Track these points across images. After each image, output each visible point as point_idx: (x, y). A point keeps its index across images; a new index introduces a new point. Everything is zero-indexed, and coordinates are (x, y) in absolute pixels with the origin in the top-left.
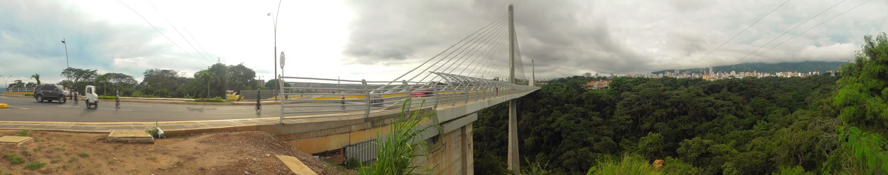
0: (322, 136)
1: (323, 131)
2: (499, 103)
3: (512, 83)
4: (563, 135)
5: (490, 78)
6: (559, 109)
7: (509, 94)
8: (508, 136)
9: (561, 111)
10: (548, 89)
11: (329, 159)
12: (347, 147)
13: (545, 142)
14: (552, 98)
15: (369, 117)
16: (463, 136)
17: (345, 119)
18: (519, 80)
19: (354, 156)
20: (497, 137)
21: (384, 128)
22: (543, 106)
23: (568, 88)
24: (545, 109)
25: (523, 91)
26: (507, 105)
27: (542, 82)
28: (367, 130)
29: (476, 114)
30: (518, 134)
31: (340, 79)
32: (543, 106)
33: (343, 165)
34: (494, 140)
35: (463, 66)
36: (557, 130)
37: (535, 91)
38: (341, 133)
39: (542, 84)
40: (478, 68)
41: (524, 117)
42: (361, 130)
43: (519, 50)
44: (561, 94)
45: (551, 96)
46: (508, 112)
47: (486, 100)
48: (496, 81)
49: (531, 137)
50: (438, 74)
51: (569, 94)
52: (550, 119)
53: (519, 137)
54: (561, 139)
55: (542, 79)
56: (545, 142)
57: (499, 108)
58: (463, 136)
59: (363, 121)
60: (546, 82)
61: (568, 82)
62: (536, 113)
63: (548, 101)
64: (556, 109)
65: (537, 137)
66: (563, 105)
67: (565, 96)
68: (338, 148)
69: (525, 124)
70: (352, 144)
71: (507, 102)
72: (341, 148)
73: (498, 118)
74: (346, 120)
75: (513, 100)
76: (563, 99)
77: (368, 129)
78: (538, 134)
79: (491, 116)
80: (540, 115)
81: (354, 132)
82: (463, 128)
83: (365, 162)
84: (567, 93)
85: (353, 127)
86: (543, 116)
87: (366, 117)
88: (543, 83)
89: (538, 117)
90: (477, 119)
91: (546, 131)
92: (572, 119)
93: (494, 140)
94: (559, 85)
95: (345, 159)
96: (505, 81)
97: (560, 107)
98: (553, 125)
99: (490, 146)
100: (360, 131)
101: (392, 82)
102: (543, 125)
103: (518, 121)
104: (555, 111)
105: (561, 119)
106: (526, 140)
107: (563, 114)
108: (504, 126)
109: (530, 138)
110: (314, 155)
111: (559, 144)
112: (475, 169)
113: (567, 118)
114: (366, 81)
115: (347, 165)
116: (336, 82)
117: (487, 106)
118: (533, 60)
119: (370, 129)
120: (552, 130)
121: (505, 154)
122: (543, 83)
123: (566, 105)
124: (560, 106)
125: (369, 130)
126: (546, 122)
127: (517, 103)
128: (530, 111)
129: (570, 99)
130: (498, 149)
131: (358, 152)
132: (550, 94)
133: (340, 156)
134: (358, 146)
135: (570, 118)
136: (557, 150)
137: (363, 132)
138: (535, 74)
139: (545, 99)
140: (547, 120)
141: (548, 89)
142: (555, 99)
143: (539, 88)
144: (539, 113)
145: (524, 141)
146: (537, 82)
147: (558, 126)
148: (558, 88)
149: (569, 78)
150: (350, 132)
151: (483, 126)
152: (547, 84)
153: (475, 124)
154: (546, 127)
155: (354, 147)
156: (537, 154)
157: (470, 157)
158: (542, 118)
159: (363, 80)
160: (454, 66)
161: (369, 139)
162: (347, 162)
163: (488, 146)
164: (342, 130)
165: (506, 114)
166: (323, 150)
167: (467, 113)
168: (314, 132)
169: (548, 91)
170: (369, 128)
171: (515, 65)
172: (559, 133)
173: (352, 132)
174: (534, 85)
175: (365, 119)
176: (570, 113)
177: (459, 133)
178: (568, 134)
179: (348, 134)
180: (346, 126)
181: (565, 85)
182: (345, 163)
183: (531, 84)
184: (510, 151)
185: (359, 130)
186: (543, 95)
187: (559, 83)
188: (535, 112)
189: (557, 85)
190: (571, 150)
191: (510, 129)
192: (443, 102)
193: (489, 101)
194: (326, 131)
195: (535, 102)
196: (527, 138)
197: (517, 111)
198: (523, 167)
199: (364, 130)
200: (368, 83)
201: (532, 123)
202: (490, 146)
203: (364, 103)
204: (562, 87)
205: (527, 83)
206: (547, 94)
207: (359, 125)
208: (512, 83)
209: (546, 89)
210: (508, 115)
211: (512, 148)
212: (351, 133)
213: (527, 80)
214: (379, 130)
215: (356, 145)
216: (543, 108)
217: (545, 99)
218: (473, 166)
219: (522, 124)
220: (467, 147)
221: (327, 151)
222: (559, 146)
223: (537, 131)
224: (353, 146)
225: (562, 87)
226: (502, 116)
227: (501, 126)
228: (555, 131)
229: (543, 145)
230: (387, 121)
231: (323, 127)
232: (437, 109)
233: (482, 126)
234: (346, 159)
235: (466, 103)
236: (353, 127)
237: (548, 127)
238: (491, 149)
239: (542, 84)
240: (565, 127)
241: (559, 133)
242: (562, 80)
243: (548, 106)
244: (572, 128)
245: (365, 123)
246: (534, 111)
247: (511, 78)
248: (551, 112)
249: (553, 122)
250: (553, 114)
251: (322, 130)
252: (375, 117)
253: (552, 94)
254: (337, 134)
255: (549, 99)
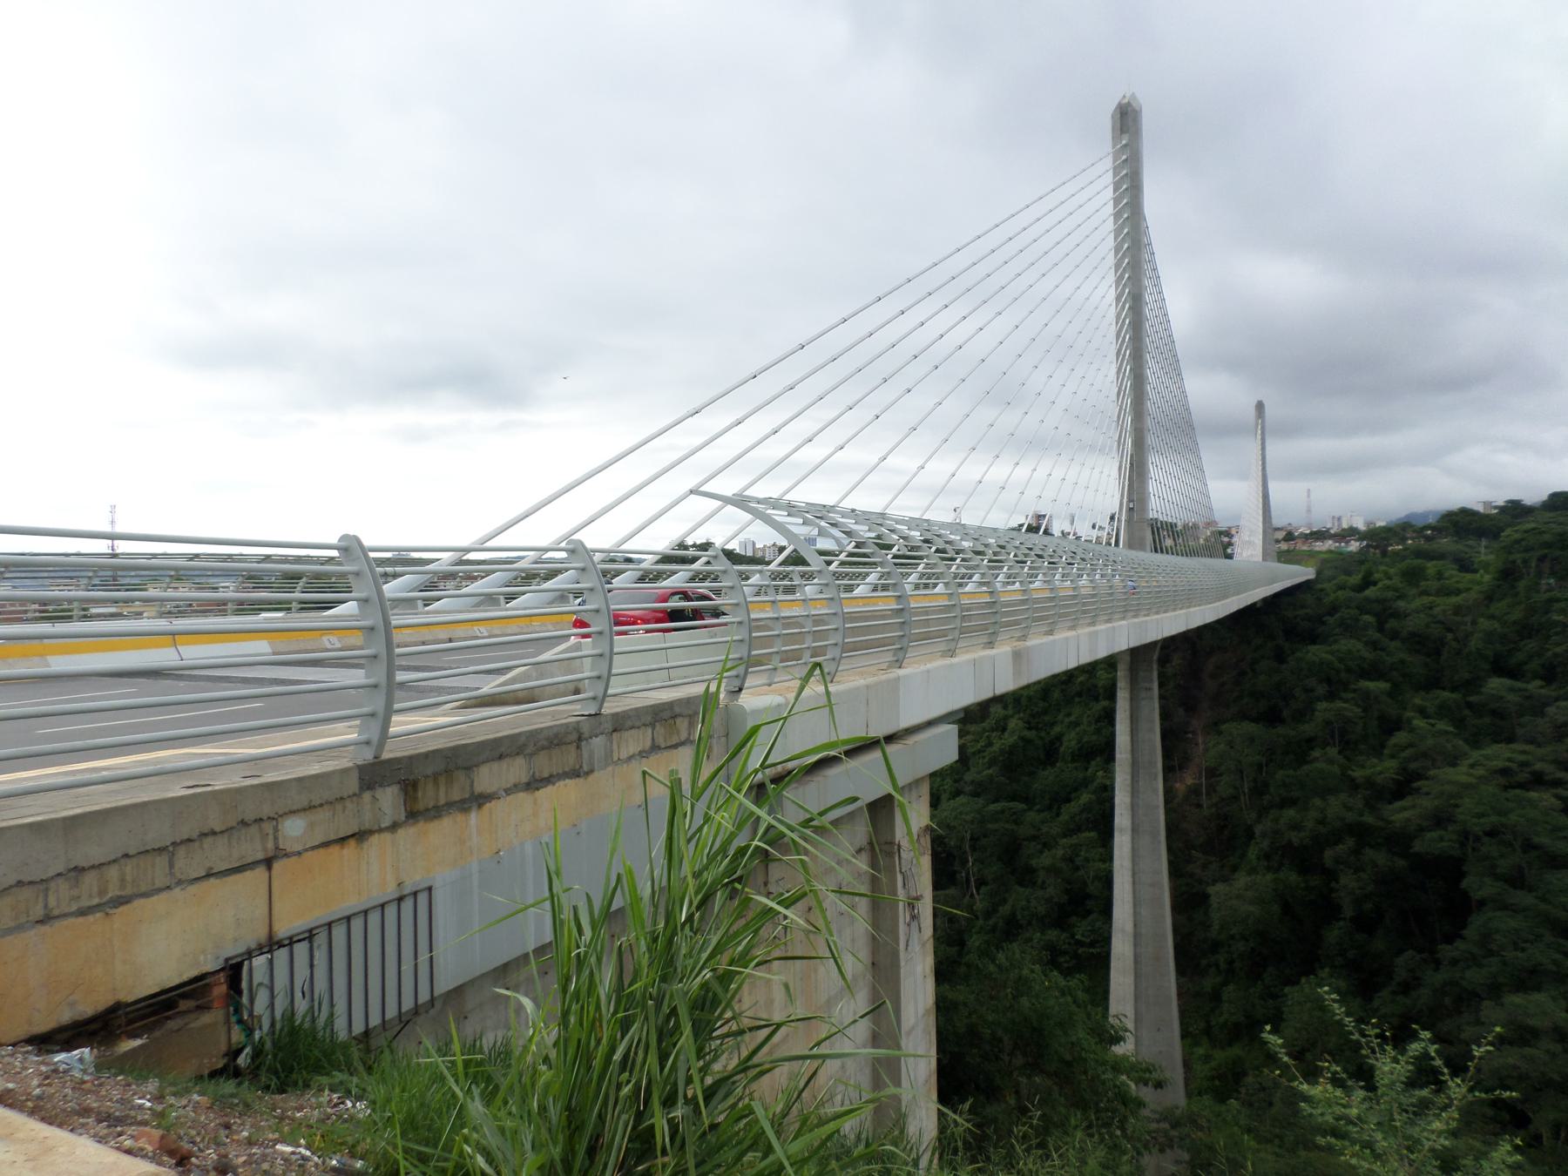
0: (82, 913)
1: (90, 879)
2: (1072, 664)
3: (1131, 545)
4: (1477, 885)
5: (1001, 517)
6: (1443, 711)
7: (1125, 613)
8: (1108, 857)
9: (1460, 723)
10: (1367, 582)
11: (134, 1051)
12: (249, 954)
13: (1348, 911)
14: (1394, 635)
15: (386, 756)
16: (881, 850)
17: (233, 780)
18: (1173, 526)
19: (301, 1006)
20: (1045, 859)
21: (473, 817)
22: (1335, 686)
23: (1508, 575)
24: (1347, 707)
25: (1189, 597)
26: (1102, 676)
27: (1320, 535)
28: (375, 839)
29: (953, 729)
30: (1169, 849)
31: (120, 528)
32: (1335, 686)
33: (229, 1070)
34: (1027, 877)
35: (858, 455)
36: (1435, 842)
37: (1277, 596)
38: (209, 875)
39: (1320, 546)
40: (939, 468)
41: (1205, 749)
42: (342, 840)
43: (1168, 329)
44: (1458, 610)
45: (1392, 624)
46: (1109, 717)
47: (1003, 650)
48: (1037, 539)
49: (1252, 871)
50: (740, 501)
51: (1517, 615)
52: (1384, 768)
53: (1175, 871)
54: (1460, 909)
55: (1322, 518)
56: (1348, 911)
57: (1056, 695)
58: (881, 850)
59: (353, 784)
60: (1352, 532)
61: (1509, 534)
62: (1281, 730)
63: (1367, 654)
64: (1423, 712)
65: (1293, 877)
66: (1472, 685)
67: (1484, 624)
68: (194, 973)
69: (1211, 789)
70: (283, 930)
71: (1110, 662)
72: (210, 967)
73: (1050, 755)
74: (239, 791)
75: (1138, 655)
76: (1475, 643)
77: (381, 830)
78: (1304, 858)
79: (1009, 739)
80: (1310, 742)
81: (299, 853)
82: (881, 809)
83: (367, 1033)
84: (1498, 607)
85: (294, 829)
86: (1333, 752)
87: (367, 755)
88: (1329, 544)
89: (1300, 751)
90: (952, 756)
91: (1350, 842)
92: (1538, 780)
93: (1027, 877)
94: (1441, 556)
95: (237, 1035)
96: (1095, 534)
97: (1446, 694)
98: (1401, 814)
99: (1005, 910)
100: (335, 849)
101: (547, 550)
102: (1335, 807)
103: (1171, 769)
104: (1419, 723)
105: (1460, 774)
106: (1217, 891)
107: (1475, 743)
108: (1085, 797)
109: (1242, 880)
110: (45, 1042)
111: (1449, 939)
112: (944, 1040)
113: (1504, 772)
114: (367, 542)
115: (254, 1071)
116: (101, 546)
117: (1006, 683)
118: (1260, 407)
119: (394, 827)
120: (1398, 841)
121: (1096, 963)
122: (1329, 544)
123: (1496, 684)
124: (1454, 689)
125: (387, 836)
126: (1354, 786)
127: (1163, 662)
128: (1243, 716)
129: (1531, 645)
130: (1053, 934)
131: (321, 985)
132: (1385, 613)
133: (206, 1018)
134: (321, 939)
135: (1523, 777)
136: (1434, 978)
137: (350, 849)
138: (1273, 486)
139: (1346, 644)
140: (1358, 774)
141: (1367, 582)
142: (1418, 642)
143: (1302, 573)
144: (1308, 729)
145: (1206, 897)
146: (1289, 537)
147: (1440, 820)
148: (1440, 576)
149: (1515, 510)
150: (268, 863)
151: (962, 799)
152: (1354, 546)
153: (943, 786)
154: (1351, 817)
155: (301, 949)
156: (1293, 981)
157: (919, 969)
158: (1325, 760)
159: (344, 538)
160: (812, 454)
161: (391, 891)
162: (258, 1053)
163: (988, 914)
164: (218, 854)
165: (1098, 731)
166: (88, 1007)
167: (905, 723)
168: (26, 893)
169: (1370, 592)
170: (386, 823)
171: (1150, 440)
172: (1449, 869)
173: (287, 855)
174: (1265, 556)
175: (362, 769)
176: (1531, 741)
177: (861, 831)
178: (1516, 880)
179: (260, 873)
180: (244, 823)
181: (1484, 552)
182: (243, 1060)
183: (1250, 548)
184: (1121, 948)
185: (326, 845)
186: (1331, 620)
187: (1445, 543)
188: (1282, 721)
189: (1429, 556)
190: (1538, 988)
191: (1122, 819)
192: (776, 662)
193: (1017, 656)
194: (113, 873)
195: (1280, 657)
196: (1225, 880)
197: (1165, 716)
198: (1201, 1051)
199: (361, 836)
200: (372, 555)
201: (1259, 790)
202: (1005, 910)
203: (357, 677)
204: (1465, 566)
205: (1221, 543)
206: (1362, 609)
207: (322, 815)
208: (1131, 545)
209: (1355, 579)
210: (1113, 735)
211: (1137, 936)
212: (277, 866)
213: (1223, 526)
214: (440, 832)
215: (310, 935)
216: (1331, 696)
217: (1346, 644)
218: (932, 1020)
219: (1195, 791)
220: (903, 915)
221: (116, 1007)
222: (1447, 951)
223: (1295, 837)
224: (291, 942)
225: (1465, 566)
226: (1070, 742)
227: (1069, 800)
228: (1418, 847)
229: (1334, 934)
230: (487, 778)
231: (92, 851)
232: (748, 701)
233: (957, 793)
234: (249, 1031)
235: (899, 663)
236: (294, 829)
237: (1369, 819)
238: (1011, 929)
239: (1320, 546)
240: (1491, 833)
241: (1449, 869)
242: (1462, 523)
243: (1371, 685)
244: (1543, 840)
245: (367, 796)
246: (1272, 718)
247: (1129, 521)
248: (1391, 726)
249: (1403, 787)
250: (1400, 737)
251: (80, 870)
252: (427, 755)
253: (1397, 615)
254: (179, 882)
255: (1375, 645)
